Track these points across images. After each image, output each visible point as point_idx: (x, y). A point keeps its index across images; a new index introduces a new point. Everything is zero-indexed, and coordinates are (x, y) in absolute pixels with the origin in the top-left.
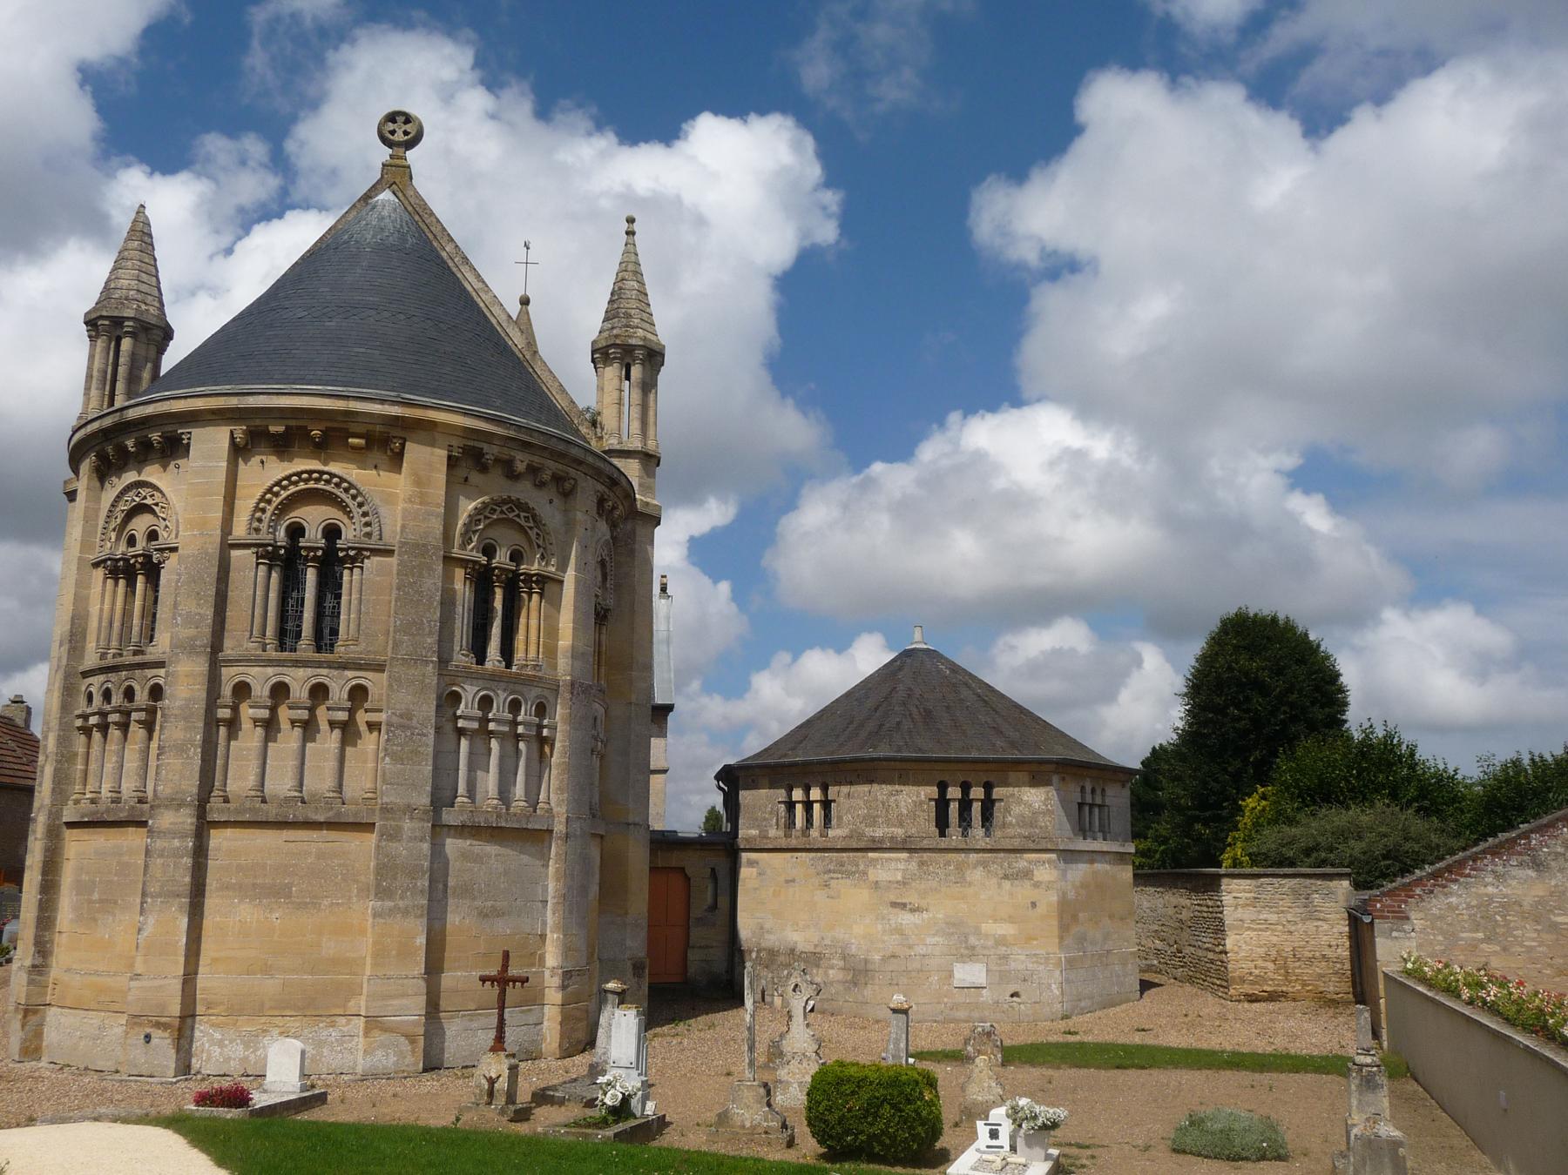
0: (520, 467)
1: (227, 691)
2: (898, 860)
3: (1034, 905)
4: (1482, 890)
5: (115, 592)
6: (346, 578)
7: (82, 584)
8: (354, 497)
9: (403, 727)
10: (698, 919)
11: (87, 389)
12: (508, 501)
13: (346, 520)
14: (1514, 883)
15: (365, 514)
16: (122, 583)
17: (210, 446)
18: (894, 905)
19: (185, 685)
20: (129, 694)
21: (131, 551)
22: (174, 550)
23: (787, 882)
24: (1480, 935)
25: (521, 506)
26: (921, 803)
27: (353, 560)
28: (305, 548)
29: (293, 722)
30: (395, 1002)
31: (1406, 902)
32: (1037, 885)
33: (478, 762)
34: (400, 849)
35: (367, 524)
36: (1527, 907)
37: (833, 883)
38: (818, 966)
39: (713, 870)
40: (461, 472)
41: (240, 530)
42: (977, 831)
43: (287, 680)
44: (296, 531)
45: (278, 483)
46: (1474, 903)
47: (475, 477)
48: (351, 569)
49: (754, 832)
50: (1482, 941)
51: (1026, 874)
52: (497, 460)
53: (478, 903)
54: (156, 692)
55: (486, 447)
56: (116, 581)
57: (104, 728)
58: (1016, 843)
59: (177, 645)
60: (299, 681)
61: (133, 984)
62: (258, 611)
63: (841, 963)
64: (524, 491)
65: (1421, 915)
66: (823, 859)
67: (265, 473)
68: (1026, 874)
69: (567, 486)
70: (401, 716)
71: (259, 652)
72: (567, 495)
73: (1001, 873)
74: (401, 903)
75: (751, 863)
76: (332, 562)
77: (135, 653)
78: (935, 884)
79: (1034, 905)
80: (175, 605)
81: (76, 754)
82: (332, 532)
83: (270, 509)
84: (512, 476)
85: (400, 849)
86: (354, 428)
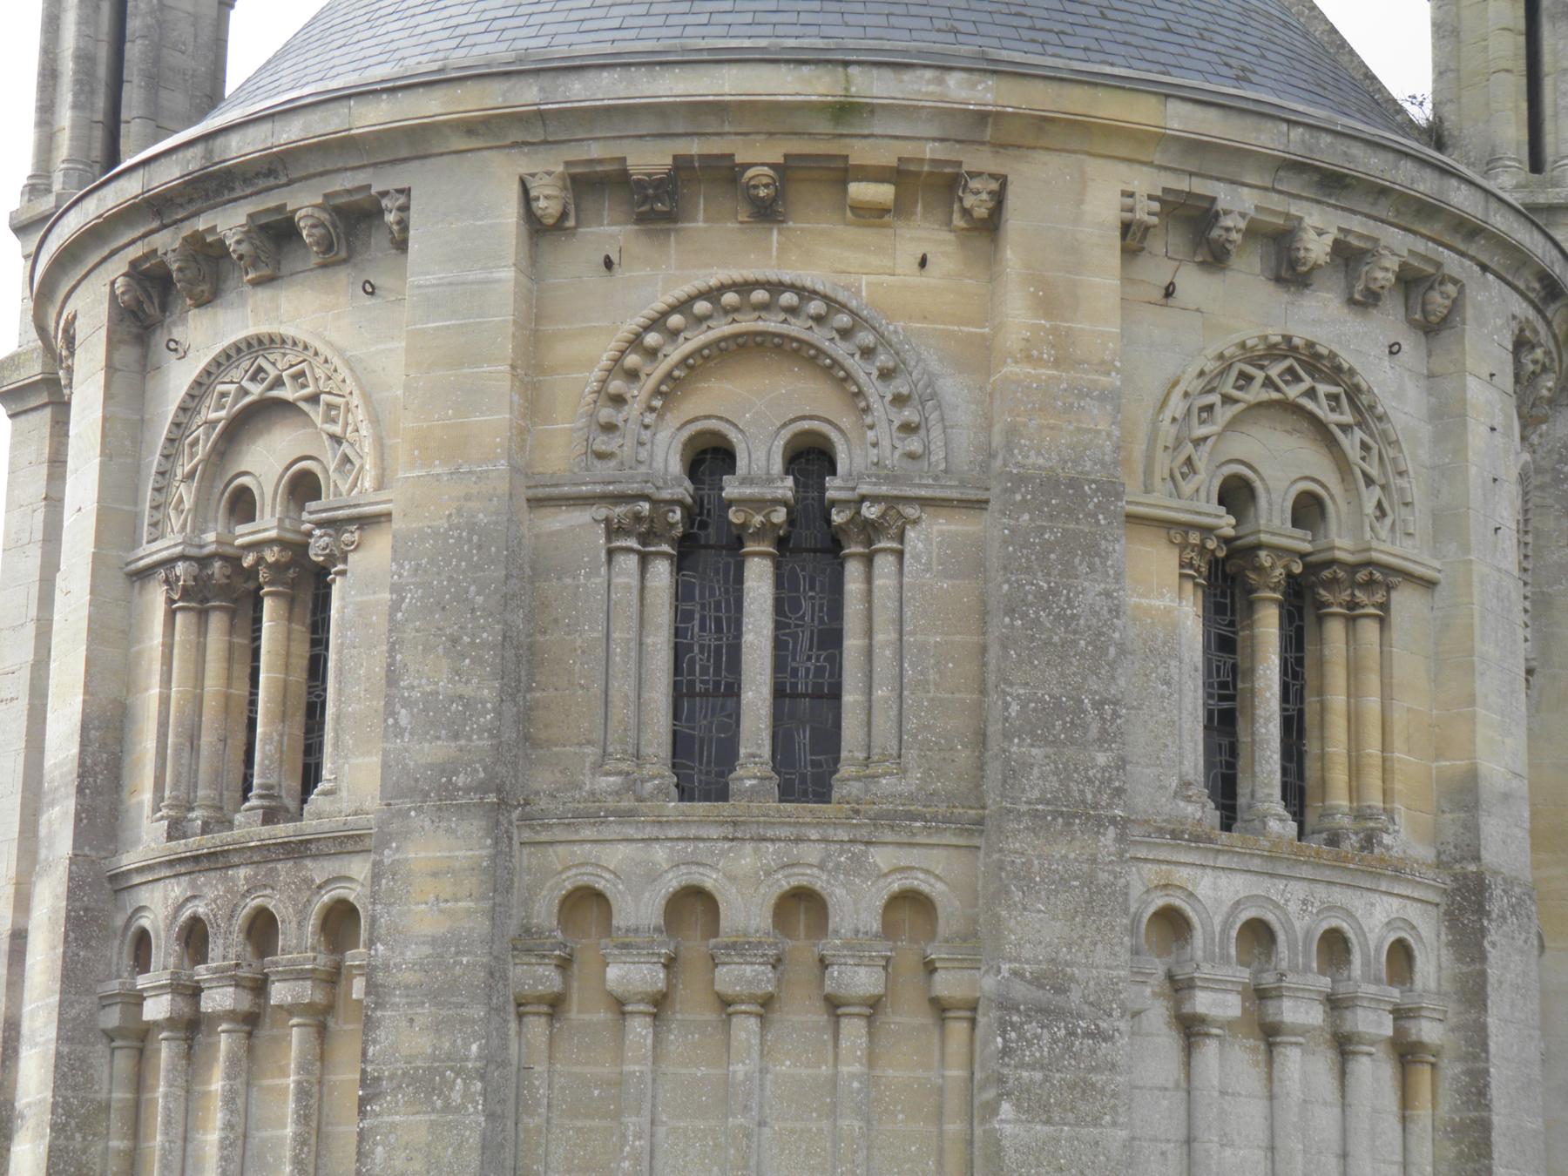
0: (1316, 248)
5: (201, 649)
6: (853, 584)
7: (111, 637)
8: (867, 353)
9: (1044, 1012)
11: (46, 109)
12: (1285, 348)
13: (846, 422)
15: (900, 400)
16: (217, 622)
17: (466, 226)
19: (427, 895)
20: (262, 929)
21: (244, 534)
22: (366, 522)
25: (1315, 362)
27: (870, 531)
28: (741, 502)
40: (1154, 271)
44: (710, 457)
45: (657, 322)
47: (1194, 284)
48: (869, 560)
52: (1254, 232)
54: (340, 922)
55: (1224, 196)
56: (203, 614)
57: (192, 1027)
59: (404, 789)
64: (1319, 317)
69: (1438, 302)
70: (1037, 981)
72: (1432, 328)
76: (817, 544)
77: (270, 817)
80: (392, 676)
81: (106, 1107)
82: (810, 457)
83: (639, 394)
84: (1290, 273)
86: (861, 153)
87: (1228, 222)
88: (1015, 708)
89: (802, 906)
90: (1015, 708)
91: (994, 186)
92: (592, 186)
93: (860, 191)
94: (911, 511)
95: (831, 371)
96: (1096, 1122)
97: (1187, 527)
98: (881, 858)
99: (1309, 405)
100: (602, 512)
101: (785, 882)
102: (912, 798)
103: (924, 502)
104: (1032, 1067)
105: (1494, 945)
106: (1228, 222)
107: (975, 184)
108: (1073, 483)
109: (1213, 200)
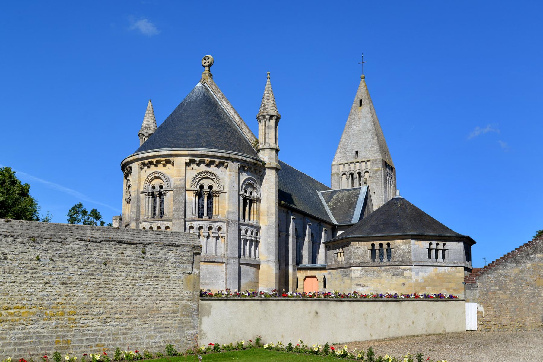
2: (358, 270)
3: (404, 284)
4: (499, 271)
14: (509, 268)
18: (357, 285)
24: (498, 288)
26: (366, 251)
31: (475, 277)
32: (405, 277)
33: (245, 244)
36: (512, 277)
41: (188, 187)
42: (385, 260)
44: (202, 187)
46: (496, 276)
50: (498, 290)
51: (401, 274)
58: (397, 263)
62: (147, 209)
65: (479, 281)
67: (194, 170)
68: (401, 274)
73: (392, 273)
76: (161, 195)
78: (369, 277)
79: (404, 284)
82: (211, 187)
89: (159, 228)
92: (144, 164)
93: (162, 162)
95: (161, 179)
98: (165, 223)
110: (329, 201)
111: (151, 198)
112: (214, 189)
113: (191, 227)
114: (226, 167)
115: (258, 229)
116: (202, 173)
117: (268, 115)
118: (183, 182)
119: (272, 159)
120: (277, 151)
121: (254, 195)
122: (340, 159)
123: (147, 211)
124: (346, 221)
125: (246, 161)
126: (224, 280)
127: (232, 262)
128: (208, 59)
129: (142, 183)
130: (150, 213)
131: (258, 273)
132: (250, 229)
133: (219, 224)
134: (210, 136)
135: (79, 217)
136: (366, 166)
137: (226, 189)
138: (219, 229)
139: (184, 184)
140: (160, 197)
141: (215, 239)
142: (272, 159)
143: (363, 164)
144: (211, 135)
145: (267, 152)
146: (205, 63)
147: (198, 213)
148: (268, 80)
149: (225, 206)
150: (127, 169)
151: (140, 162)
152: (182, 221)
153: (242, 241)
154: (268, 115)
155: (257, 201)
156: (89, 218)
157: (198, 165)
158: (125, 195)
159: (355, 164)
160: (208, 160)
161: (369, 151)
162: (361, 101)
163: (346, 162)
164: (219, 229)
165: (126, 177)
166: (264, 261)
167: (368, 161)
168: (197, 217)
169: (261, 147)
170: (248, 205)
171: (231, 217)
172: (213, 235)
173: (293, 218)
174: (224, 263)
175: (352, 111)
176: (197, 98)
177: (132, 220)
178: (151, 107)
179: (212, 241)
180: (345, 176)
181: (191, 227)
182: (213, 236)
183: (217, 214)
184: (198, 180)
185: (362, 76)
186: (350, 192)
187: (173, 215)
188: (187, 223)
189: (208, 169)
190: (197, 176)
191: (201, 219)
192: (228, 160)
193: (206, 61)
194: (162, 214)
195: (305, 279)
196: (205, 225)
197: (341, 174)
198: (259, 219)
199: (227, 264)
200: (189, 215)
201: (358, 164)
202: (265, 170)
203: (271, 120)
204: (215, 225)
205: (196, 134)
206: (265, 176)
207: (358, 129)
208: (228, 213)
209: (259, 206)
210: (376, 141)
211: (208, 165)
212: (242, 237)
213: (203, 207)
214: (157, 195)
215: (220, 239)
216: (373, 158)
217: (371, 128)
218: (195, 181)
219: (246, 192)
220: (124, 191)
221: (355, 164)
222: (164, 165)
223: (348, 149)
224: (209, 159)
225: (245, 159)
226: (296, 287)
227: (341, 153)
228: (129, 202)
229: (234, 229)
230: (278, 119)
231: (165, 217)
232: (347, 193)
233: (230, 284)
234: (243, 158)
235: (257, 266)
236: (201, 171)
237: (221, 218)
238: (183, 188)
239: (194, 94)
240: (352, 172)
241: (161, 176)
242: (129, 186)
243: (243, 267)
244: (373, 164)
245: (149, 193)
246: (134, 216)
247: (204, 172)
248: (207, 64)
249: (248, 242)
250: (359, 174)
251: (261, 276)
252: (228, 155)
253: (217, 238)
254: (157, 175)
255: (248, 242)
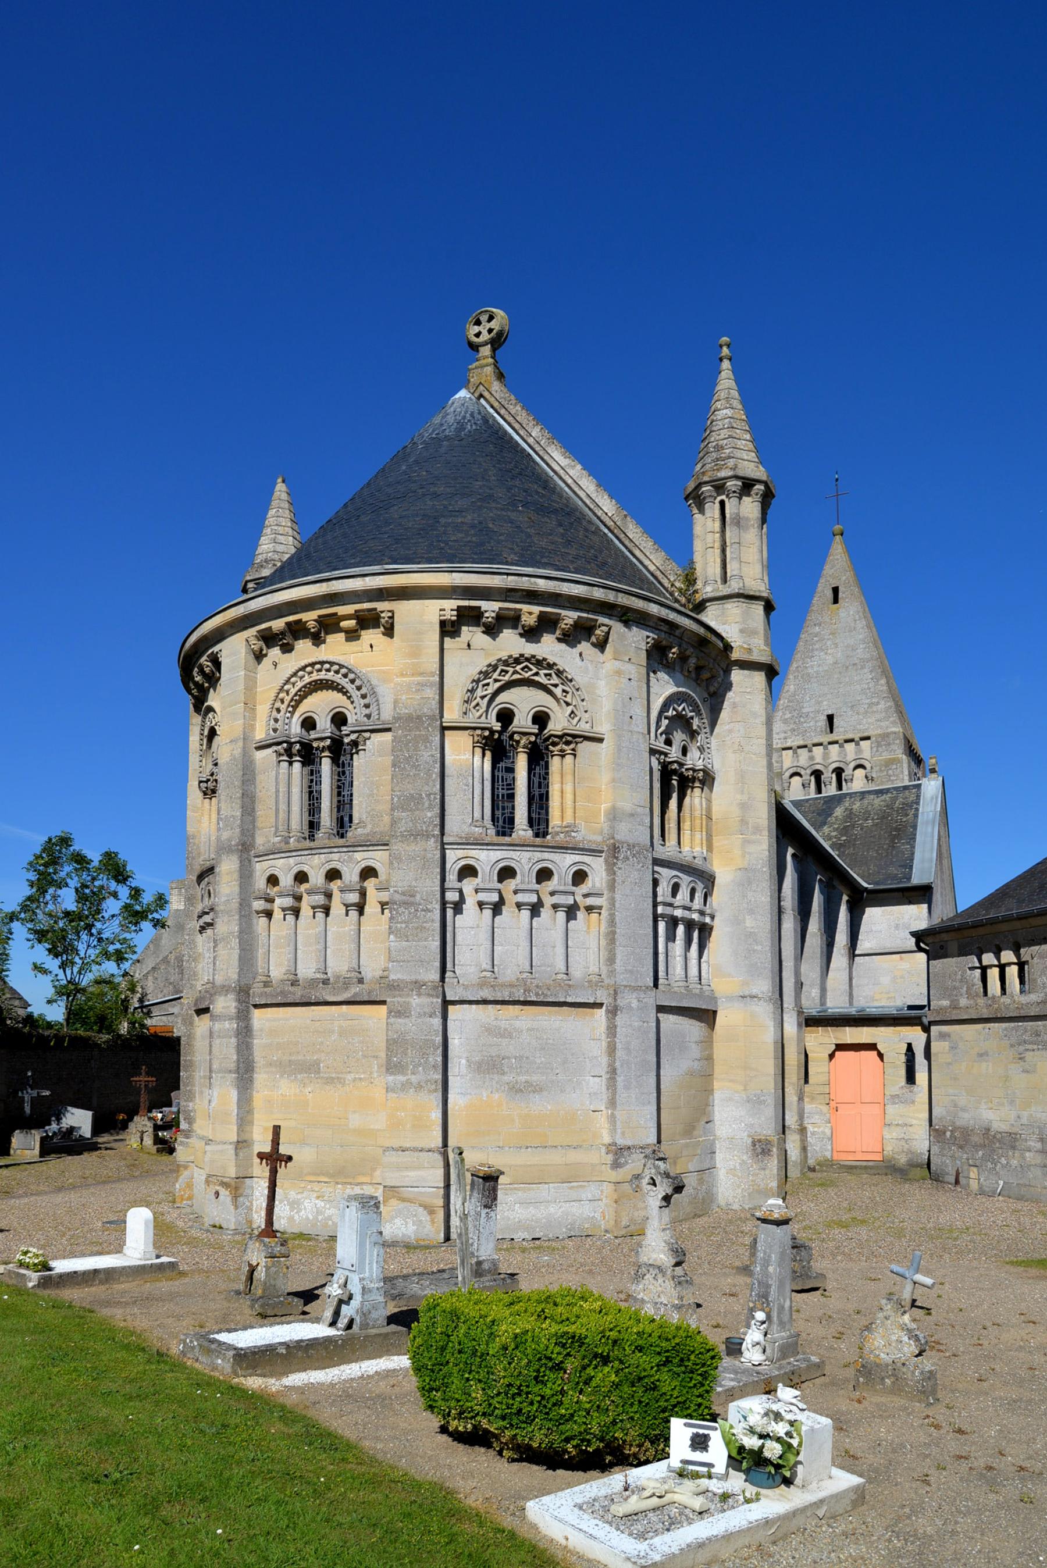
1: (261, 883)
8: (352, 681)
9: (406, 904)
10: (893, 1097)
23: (981, 1055)
29: (481, 905)
30: (412, 1174)
33: (671, 937)
34: (408, 1025)
35: (367, 706)
37: (1029, 1055)
38: (1014, 1148)
39: (910, 1045)
41: (452, 714)
43: (305, 868)
44: (506, 716)
49: (946, 1003)
53: (506, 1078)
60: (316, 867)
61: (208, 1148)
62: (283, 807)
63: (1039, 1146)
66: (1016, 1029)
67: (476, 652)
70: (403, 894)
71: (283, 844)
74: (414, 1079)
75: (943, 1036)
76: (341, 751)
82: (541, 719)
85: (408, 1025)
87: (486, 615)
88: (396, 799)
90: (396, 799)
91: (390, 614)
92: (269, 639)
93: (344, 624)
94: (367, 735)
96: (426, 940)
97: (475, 728)
98: (358, 856)
99: (536, 678)
100: (275, 748)
101: (328, 867)
102: (368, 835)
103: (372, 731)
104: (401, 923)
105: (620, 869)
106: (486, 615)
107: (382, 615)
108: (419, 717)
109: (480, 608)
110: (825, 823)
111: (297, 766)
112: (557, 725)
113: (468, 871)
114: (601, 645)
115: (708, 880)
116: (506, 663)
117: (737, 477)
118: (432, 693)
119: (753, 633)
120: (769, 607)
121: (694, 759)
122: (782, 735)
123: (282, 815)
124: (894, 877)
125: (672, 626)
126: (603, 1069)
127: (635, 1004)
128: (491, 318)
129: (263, 710)
130: (298, 819)
131: (707, 1043)
132: (685, 880)
133: (578, 858)
134: (529, 536)
135: (63, 874)
136: (859, 751)
137: (603, 728)
138: (580, 877)
139: (435, 704)
140: (335, 761)
141: (561, 916)
142: (753, 633)
143: (850, 747)
144: (532, 531)
145: (734, 608)
146: (478, 335)
147: (494, 819)
148: (726, 364)
149: (597, 790)
150: (202, 671)
151: (253, 631)
152: (432, 844)
153: (662, 926)
154: (737, 477)
155: (703, 782)
156: (94, 879)
157: (492, 631)
158: (196, 767)
159: (826, 748)
160: (530, 613)
161: (866, 712)
162: (836, 590)
163: (802, 743)
164: (580, 877)
165: (200, 705)
166: (730, 998)
167: (863, 739)
168: (492, 831)
169: (707, 591)
170: (675, 795)
171: (625, 832)
172: (556, 899)
173: (793, 855)
174: (600, 1005)
175: (812, 617)
176: (461, 426)
177: (223, 849)
178: (284, 496)
179: (551, 922)
180: (796, 778)
181: (468, 871)
182: (555, 907)
183: (569, 819)
184: (490, 690)
185: (838, 528)
186: (887, 797)
187: (394, 823)
188: (451, 855)
189: (529, 649)
190: (486, 674)
191: (507, 839)
192: (610, 616)
193: (484, 328)
194: (343, 823)
195: (832, 1056)
196: (525, 862)
197: (788, 774)
198: (710, 848)
199: (613, 1012)
200: (457, 824)
201: (834, 749)
202: (727, 672)
203: (746, 499)
204: (564, 863)
205: (473, 527)
206: (730, 695)
207: (830, 660)
208: (614, 815)
209: (709, 801)
210: (885, 688)
211: (532, 634)
212: (660, 910)
213: (511, 797)
214: (324, 751)
215: (581, 915)
216: (879, 732)
217: (867, 656)
218: (480, 692)
219: (668, 742)
220: (194, 759)
221: (826, 748)
222: (352, 635)
223: (804, 711)
224: (536, 609)
225: (672, 616)
226: (803, 1081)
227: (785, 721)
228: (210, 791)
229: (634, 877)
230: (767, 497)
231: (354, 833)
232: (878, 802)
233: (627, 1088)
234: (665, 613)
235: (707, 1016)
236: (504, 655)
237: (585, 834)
238: (432, 718)
239: (450, 419)
240: (818, 767)
241: (338, 678)
242: (213, 733)
243: (669, 1021)
244: (879, 745)
245: (291, 744)
246: (232, 835)
247: (517, 661)
248: (485, 336)
249: (681, 929)
250: (839, 772)
251: (720, 1051)
252: (610, 597)
253: (571, 912)
254: (323, 675)
255: (681, 929)
